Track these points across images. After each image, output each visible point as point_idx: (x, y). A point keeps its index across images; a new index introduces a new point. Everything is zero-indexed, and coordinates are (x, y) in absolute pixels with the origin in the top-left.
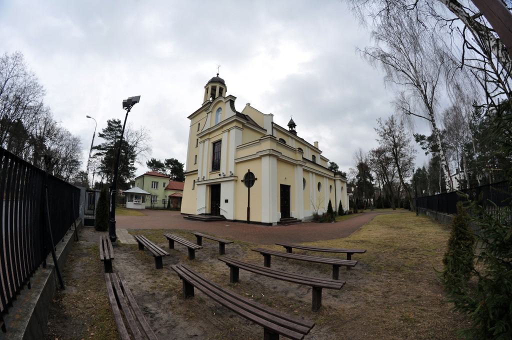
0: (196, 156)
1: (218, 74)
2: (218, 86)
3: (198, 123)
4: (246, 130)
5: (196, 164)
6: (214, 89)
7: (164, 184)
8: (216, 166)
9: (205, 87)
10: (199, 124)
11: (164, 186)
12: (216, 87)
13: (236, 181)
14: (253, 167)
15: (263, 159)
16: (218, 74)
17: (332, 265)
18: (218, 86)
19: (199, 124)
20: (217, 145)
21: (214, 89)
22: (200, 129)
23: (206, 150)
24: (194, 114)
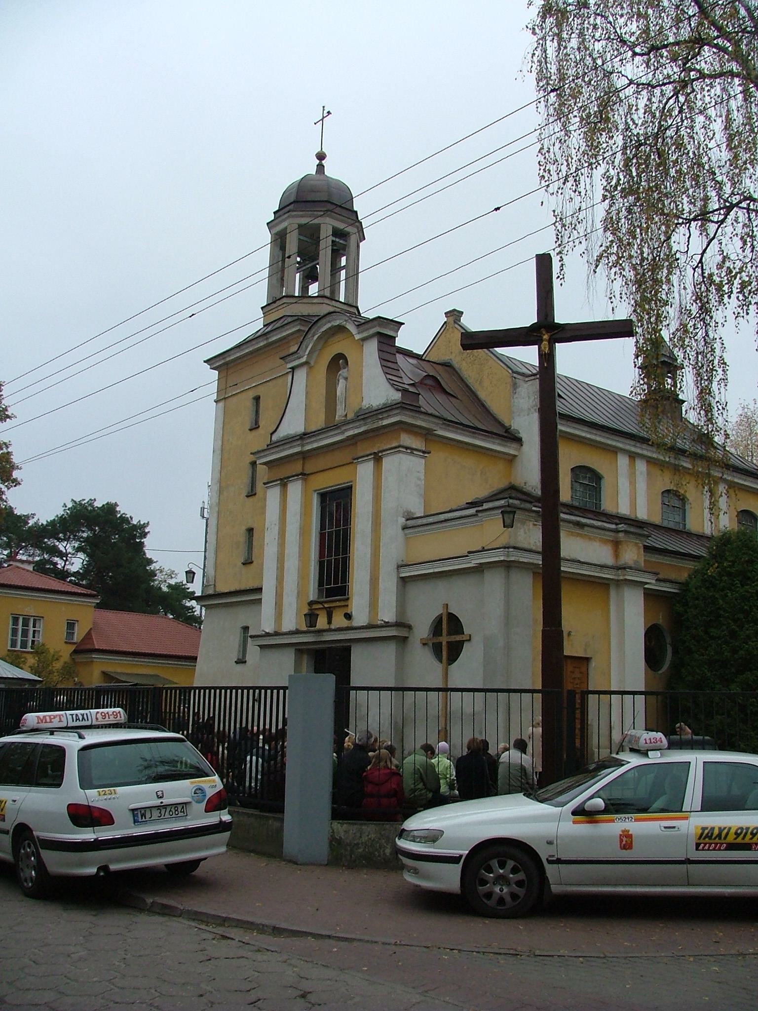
0: (250, 531)
1: (321, 156)
2: (327, 225)
3: (252, 394)
4: (439, 456)
5: (248, 563)
6: (310, 235)
7: (71, 625)
8: (333, 578)
9: (275, 213)
10: (257, 399)
11: (70, 634)
12: (318, 228)
13: (405, 639)
14: (461, 598)
15: (488, 575)
16: (321, 156)
17: (95, 783)
18: (327, 225)
19: (257, 399)
20: (336, 507)
21: (310, 235)
22: (267, 421)
23: (288, 519)
24: (215, 357)
